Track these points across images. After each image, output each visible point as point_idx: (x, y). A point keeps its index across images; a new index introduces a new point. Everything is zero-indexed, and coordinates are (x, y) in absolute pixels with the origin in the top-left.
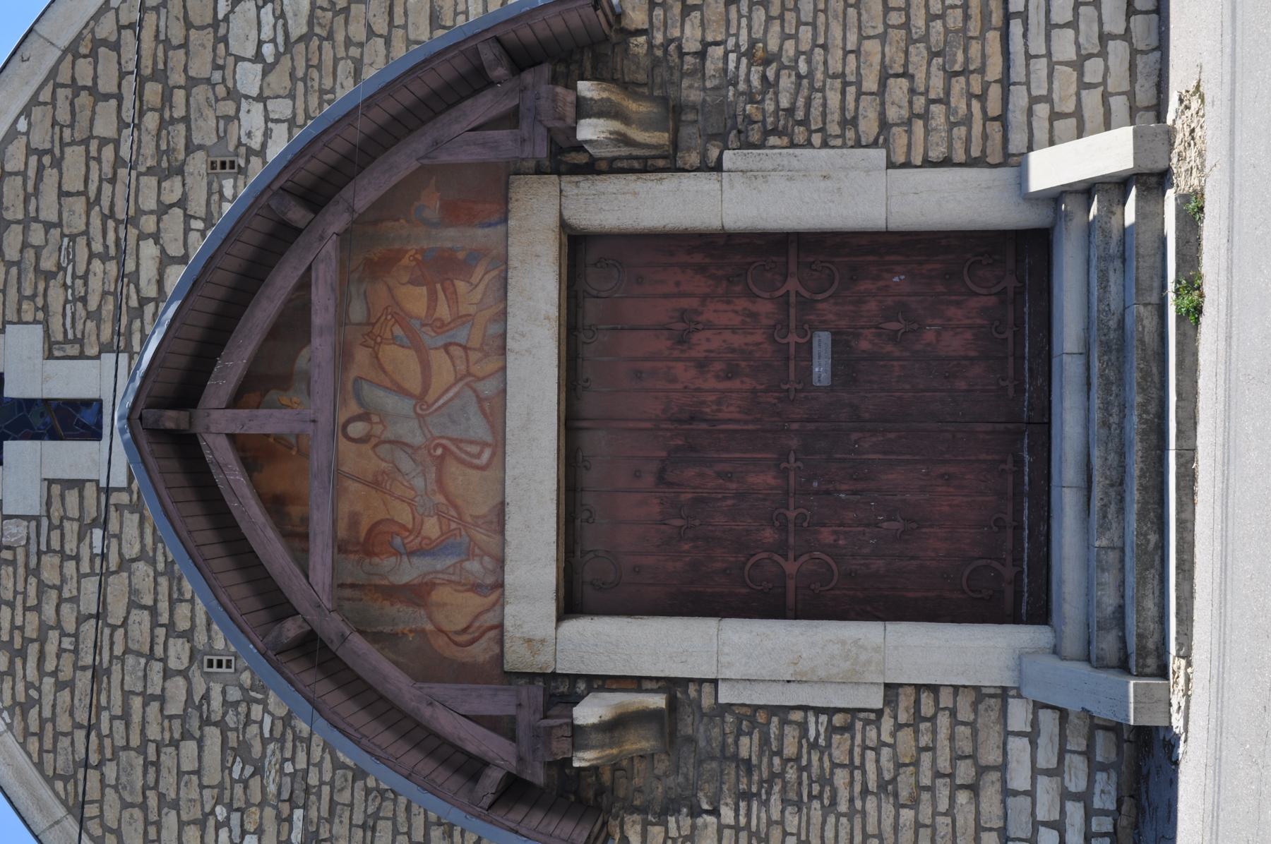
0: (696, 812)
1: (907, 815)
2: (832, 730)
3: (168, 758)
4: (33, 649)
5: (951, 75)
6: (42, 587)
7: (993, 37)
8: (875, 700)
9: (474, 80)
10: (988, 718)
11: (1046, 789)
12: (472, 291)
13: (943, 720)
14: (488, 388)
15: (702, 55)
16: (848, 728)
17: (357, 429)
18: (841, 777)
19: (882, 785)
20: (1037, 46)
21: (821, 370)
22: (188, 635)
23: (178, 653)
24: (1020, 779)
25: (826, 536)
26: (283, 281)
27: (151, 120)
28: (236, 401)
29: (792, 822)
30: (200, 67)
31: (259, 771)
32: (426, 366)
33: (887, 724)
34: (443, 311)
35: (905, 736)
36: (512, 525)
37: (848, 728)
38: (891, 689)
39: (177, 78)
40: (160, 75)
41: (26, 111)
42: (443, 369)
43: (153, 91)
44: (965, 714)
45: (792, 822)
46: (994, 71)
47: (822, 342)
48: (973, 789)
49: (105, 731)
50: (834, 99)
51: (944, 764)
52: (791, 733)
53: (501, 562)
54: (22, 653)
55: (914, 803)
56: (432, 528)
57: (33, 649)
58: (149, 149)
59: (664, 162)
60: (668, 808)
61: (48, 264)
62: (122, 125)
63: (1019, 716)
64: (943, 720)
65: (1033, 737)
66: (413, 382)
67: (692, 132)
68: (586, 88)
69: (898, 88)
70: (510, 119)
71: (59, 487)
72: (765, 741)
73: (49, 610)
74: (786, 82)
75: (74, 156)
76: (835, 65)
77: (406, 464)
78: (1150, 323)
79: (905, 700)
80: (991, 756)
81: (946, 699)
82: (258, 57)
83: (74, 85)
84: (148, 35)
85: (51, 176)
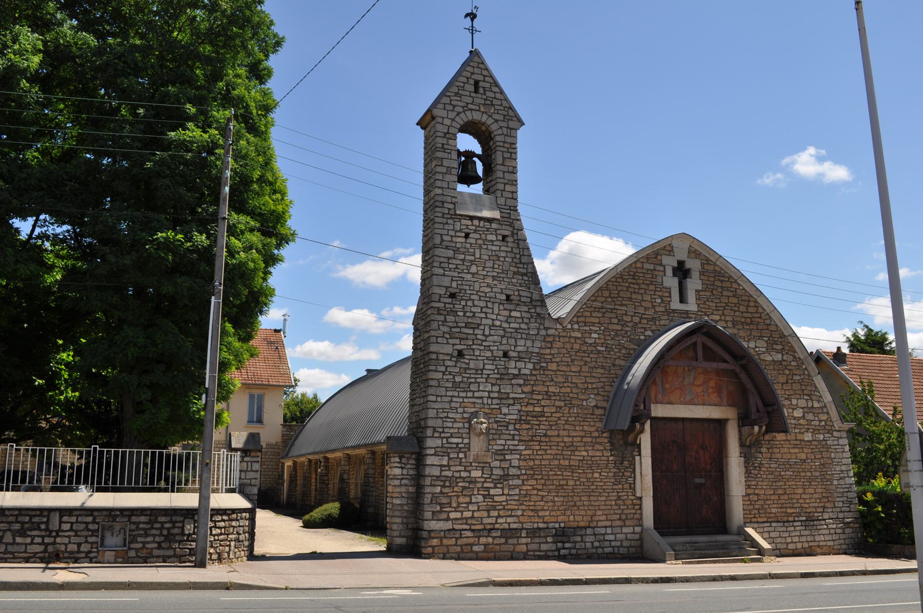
0: (611, 450)
1: (613, 503)
2: (630, 484)
3: (613, 315)
4: (634, 281)
5: (758, 509)
6: (648, 285)
7: (765, 519)
8: (638, 495)
9: (765, 404)
10: (636, 522)
11: (622, 536)
12: (714, 397)
13: (634, 511)
14: (696, 401)
15: (760, 452)
16: (630, 488)
17: (686, 369)
18: (620, 486)
19: (619, 497)
20: (766, 529)
21: (698, 480)
22: (640, 322)
23: (636, 319)
24: (625, 530)
25: (664, 482)
26: (727, 357)
27: (743, 320)
28: (703, 344)
29: (611, 474)
30: (754, 333)
31: (612, 339)
32: (699, 386)
33: (633, 498)
34: (710, 390)
35: (630, 502)
36: (669, 406)
37: (630, 488)
38: (640, 498)
39: (752, 327)
40: (752, 323)
41: (744, 289)
42: (699, 390)
43: (748, 321)
44: (636, 516)
45: (611, 474)
46: (760, 520)
47: (703, 481)
48: (620, 519)
49: (498, 248)
50: (753, 483)
51: (625, 511)
52: (629, 474)
53: (661, 403)
54: (633, 279)
55: (616, 505)
56: (667, 386)
57: (634, 281)
58: (738, 319)
59: (742, 445)
60: (612, 444)
61: (715, 292)
62: (742, 313)
63: (638, 529)
64: (634, 511)
65: (634, 533)
66: (696, 383)
67: (748, 449)
68: (764, 428)
69: (755, 498)
70: (758, 411)
71: (669, 290)
72: (627, 468)
73: (643, 286)
74: (756, 472)
75: (735, 300)
76: (760, 483)
77: (680, 380)
78: (734, 554)
79: (638, 502)
80: (627, 523)
81: (638, 512)
82: (756, 347)
83: (749, 301)
84: (759, 320)
85: (731, 294)
